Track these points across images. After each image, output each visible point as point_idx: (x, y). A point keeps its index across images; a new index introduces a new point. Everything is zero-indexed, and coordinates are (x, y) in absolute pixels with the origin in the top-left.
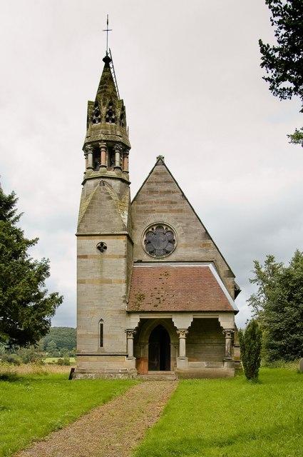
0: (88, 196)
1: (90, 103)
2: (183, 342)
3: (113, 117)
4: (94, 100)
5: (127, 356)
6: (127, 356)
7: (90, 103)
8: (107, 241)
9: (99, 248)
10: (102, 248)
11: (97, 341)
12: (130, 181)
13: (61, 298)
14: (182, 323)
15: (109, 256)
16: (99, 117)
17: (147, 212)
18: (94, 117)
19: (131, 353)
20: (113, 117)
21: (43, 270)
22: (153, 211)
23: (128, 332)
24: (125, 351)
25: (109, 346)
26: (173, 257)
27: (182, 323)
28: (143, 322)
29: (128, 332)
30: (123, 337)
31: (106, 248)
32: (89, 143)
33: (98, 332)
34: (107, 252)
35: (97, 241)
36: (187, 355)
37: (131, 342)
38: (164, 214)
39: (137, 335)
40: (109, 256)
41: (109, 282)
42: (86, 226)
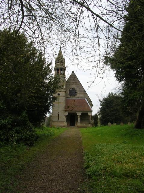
9: (58, 94)
14: (79, 114)
19: (66, 121)
23: (65, 116)
25: (60, 120)
26: (76, 97)
27: (79, 114)
28: (69, 113)
29: (65, 116)
30: (64, 117)
33: (57, 116)
34: (60, 95)
37: (66, 118)
39: (67, 117)
41: (61, 103)
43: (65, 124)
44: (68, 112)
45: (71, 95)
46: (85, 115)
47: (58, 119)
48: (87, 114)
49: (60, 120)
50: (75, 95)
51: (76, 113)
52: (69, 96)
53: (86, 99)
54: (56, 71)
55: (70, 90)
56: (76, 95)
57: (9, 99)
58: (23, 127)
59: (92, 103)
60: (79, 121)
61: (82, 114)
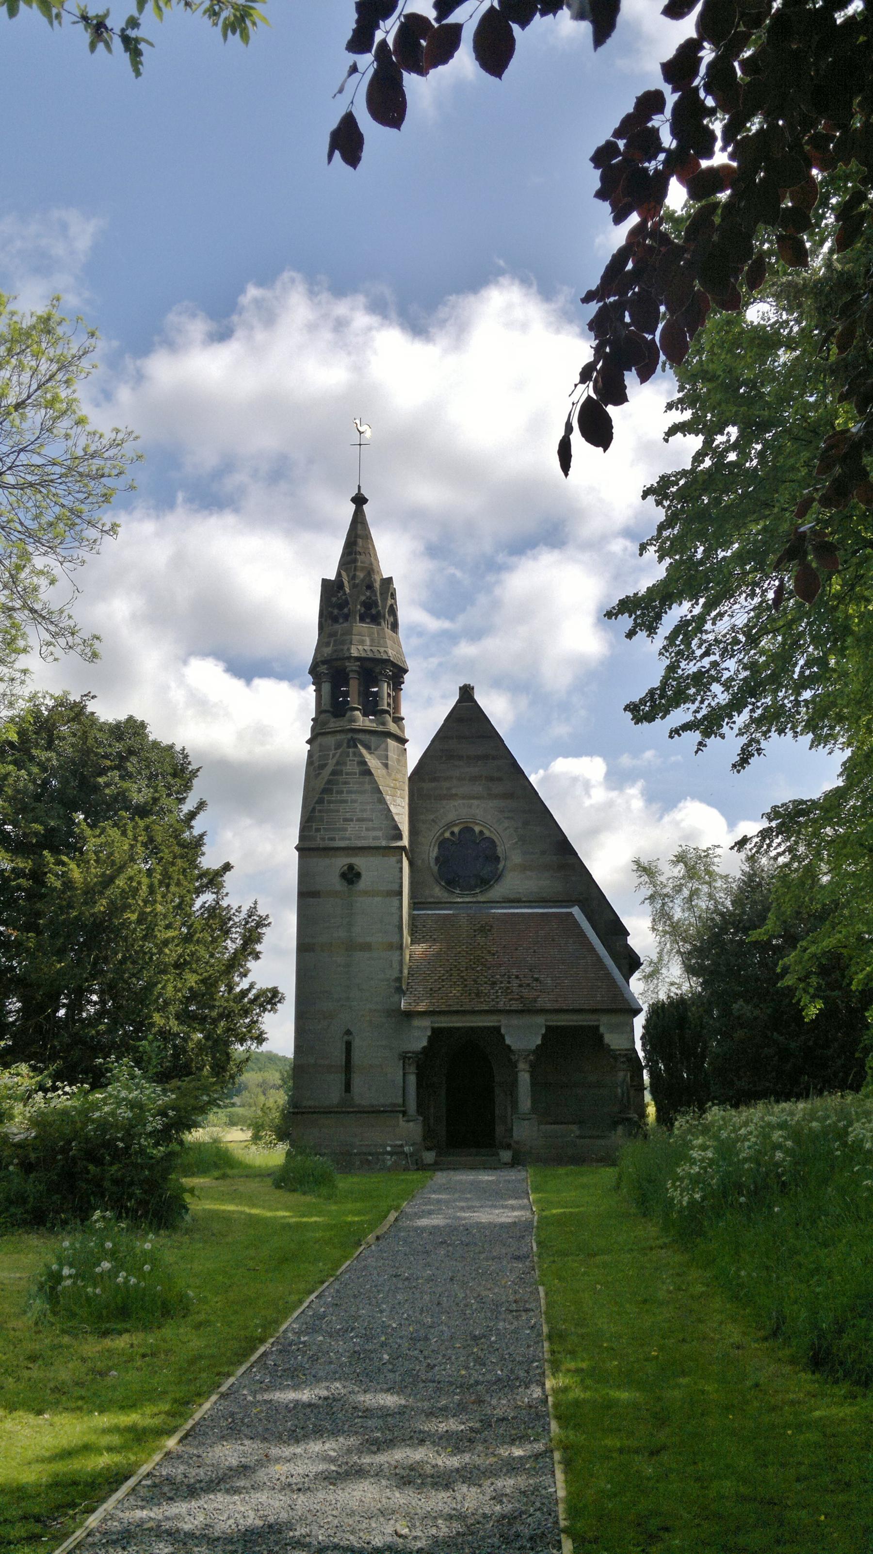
0: (322, 767)
1: (325, 582)
2: (524, 1078)
3: (374, 611)
4: (332, 576)
5: (404, 1113)
6: (404, 1113)
7: (325, 582)
8: (360, 862)
9: (343, 876)
10: (351, 876)
11: (338, 1079)
12: (407, 737)
13: (201, 836)
14: (523, 1037)
15: (366, 893)
16: (346, 610)
17: (441, 798)
18: (336, 612)
19: (412, 1105)
20: (374, 611)
21: (203, 854)
22: (453, 797)
23: (404, 1057)
24: (400, 1101)
25: (365, 1092)
26: (498, 891)
27: (523, 1037)
28: (437, 1034)
29: (404, 1057)
30: (395, 1072)
31: (358, 875)
32: (324, 662)
33: (338, 1055)
34: (363, 884)
35: (341, 862)
36: (534, 1109)
37: (412, 1079)
38: (475, 802)
39: (424, 1063)
40: (366, 893)
41: (367, 947)
42: (67, 382)
43: (408, 1131)
44: (540, 1020)
45: (451, 882)
46: (578, 1044)
47: (348, 1088)
48: (594, 1036)
49: (365, 1092)
50: (485, 882)
51: (497, 1029)
52: (438, 892)
53: (576, 911)
54: (326, 687)
55: (443, 844)
56: (498, 877)
57: (449, 789)
58: (864, 1120)
59: (628, 946)
60: (525, 1102)
61: (552, 1034)
